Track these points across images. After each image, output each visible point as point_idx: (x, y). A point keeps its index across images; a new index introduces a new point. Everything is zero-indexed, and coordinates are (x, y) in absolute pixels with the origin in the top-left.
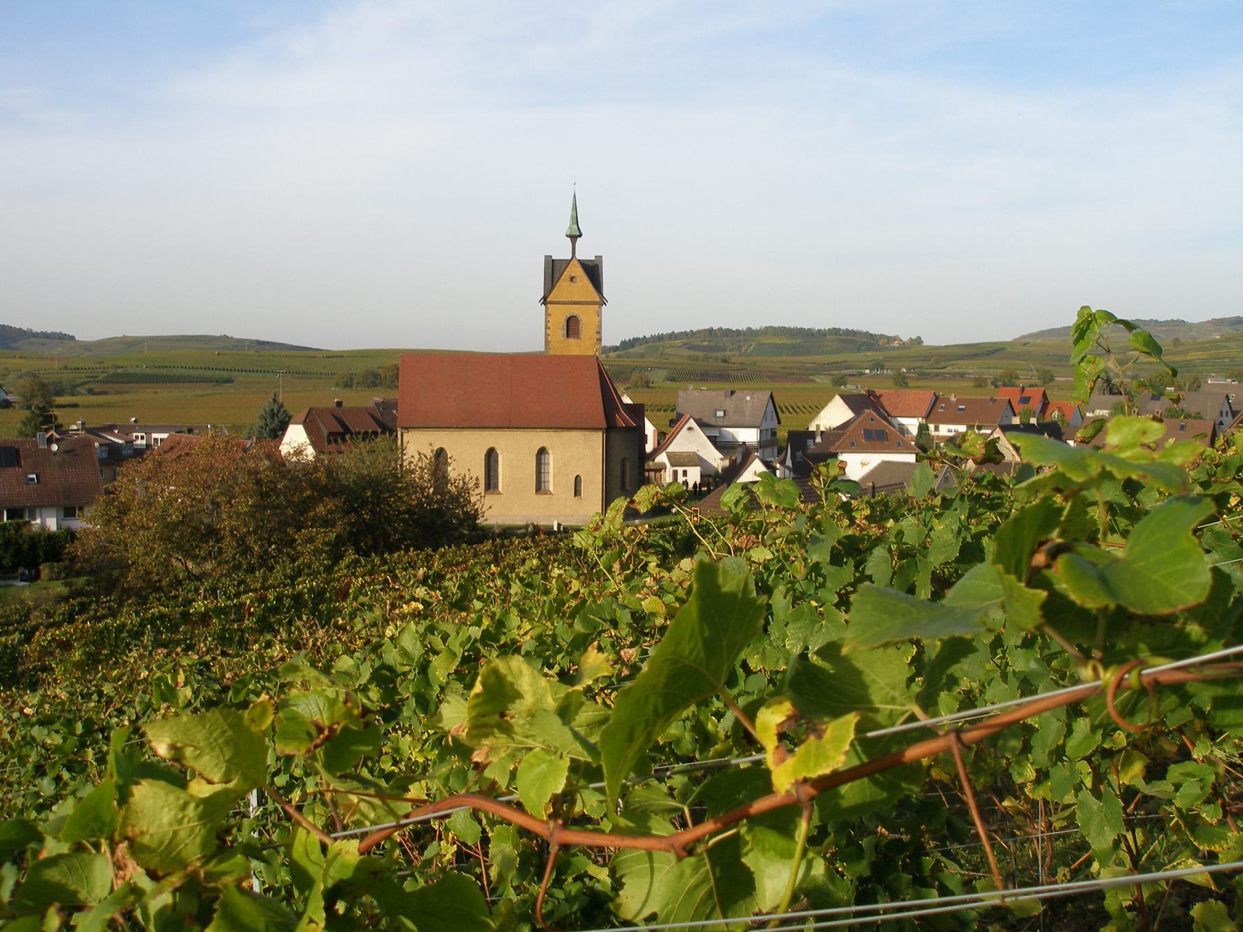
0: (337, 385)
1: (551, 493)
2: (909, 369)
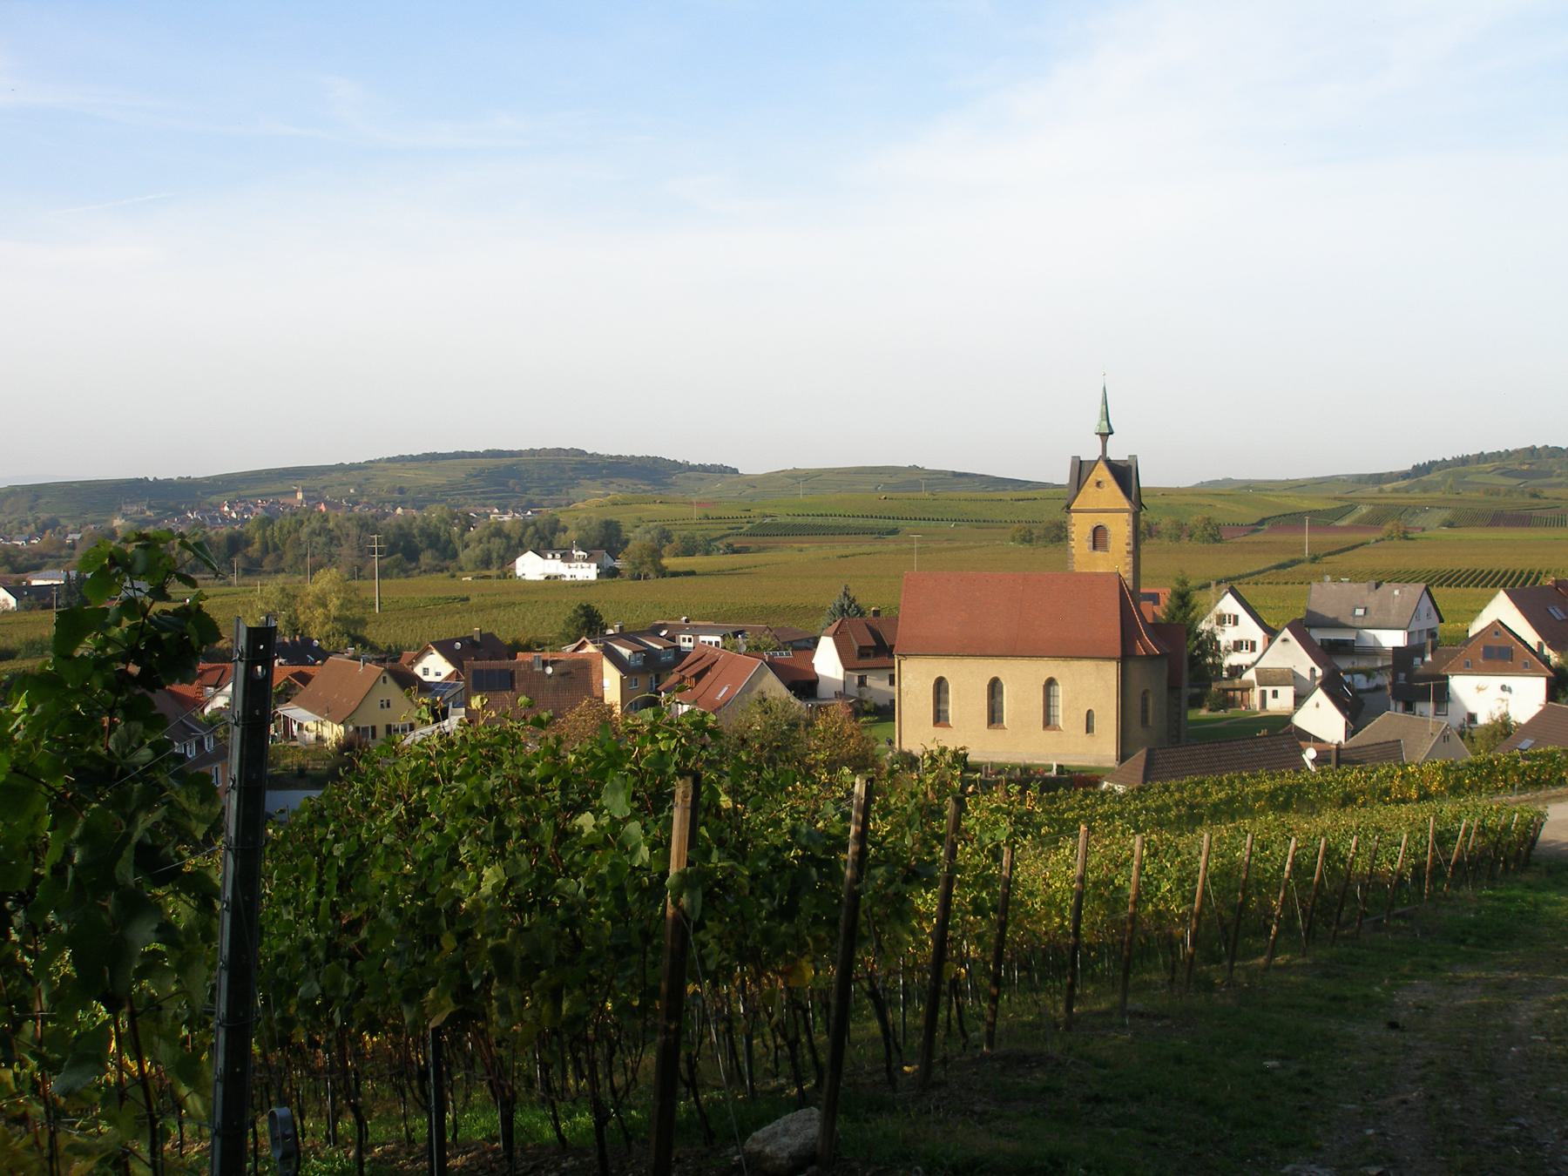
1: (1060, 729)
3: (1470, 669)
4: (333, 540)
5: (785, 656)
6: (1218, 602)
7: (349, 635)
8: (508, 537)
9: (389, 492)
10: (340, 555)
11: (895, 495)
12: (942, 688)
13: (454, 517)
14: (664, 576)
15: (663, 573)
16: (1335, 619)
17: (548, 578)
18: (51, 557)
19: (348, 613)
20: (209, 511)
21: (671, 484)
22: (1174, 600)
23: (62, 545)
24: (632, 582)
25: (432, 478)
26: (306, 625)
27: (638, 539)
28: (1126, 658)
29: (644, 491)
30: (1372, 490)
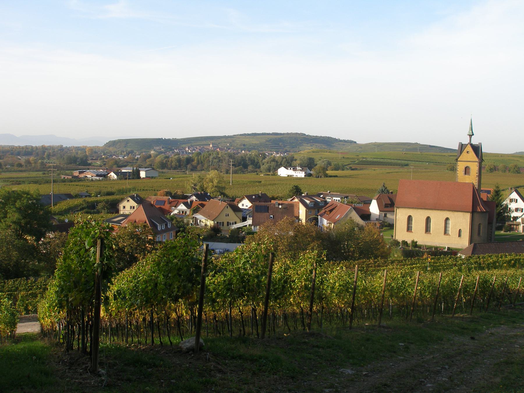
0: (447, 169)
1: (450, 235)
4: (220, 160)
5: (361, 206)
7: (220, 192)
8: (277, 162)
10: (222, 166)
12: (410, 219)
14: (327, 177)
15: (326, 176)
17: (288, 176)
18: (130, 163)
20: (181, 150)
21: (333, 146)
23: (134, 159)
24: (315, 179)
25: (254, 141)
26: (206, 188)
27: (320, 164)
28: (473, 212)
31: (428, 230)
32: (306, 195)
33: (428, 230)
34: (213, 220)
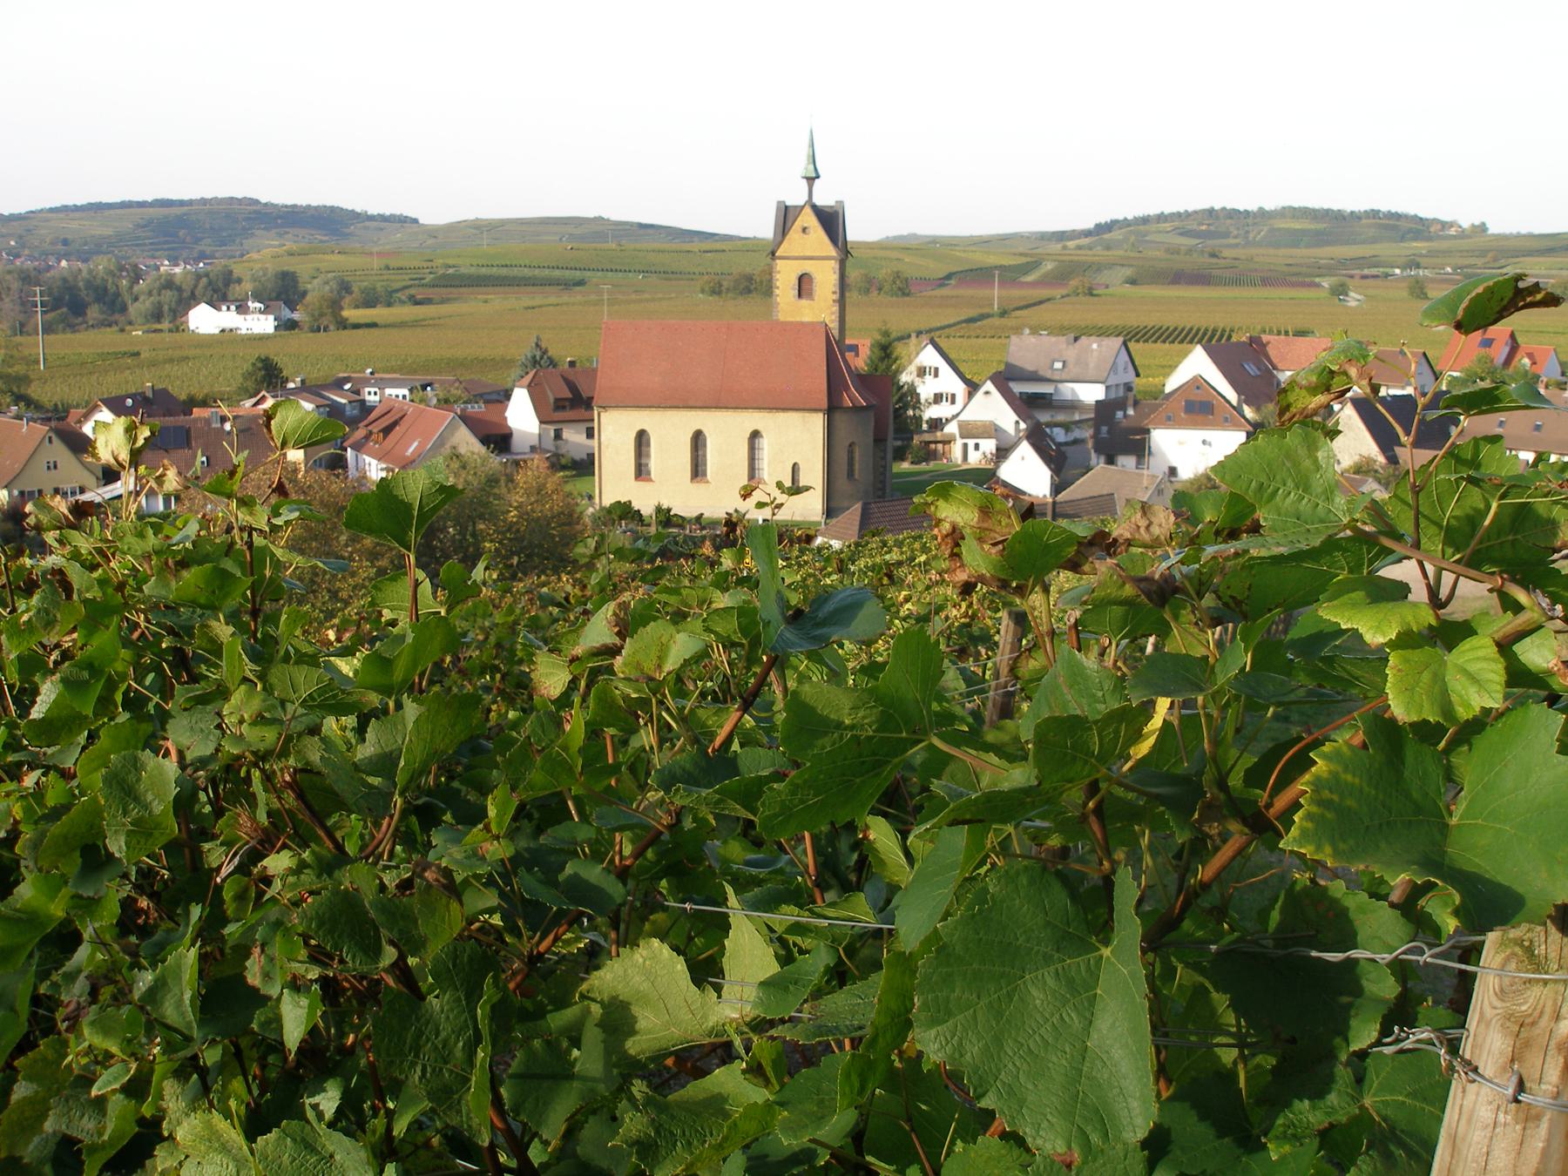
0: (703, 291)
2: (1454, 269)
3: (1170, 422)
5: (477, 409)
6: (918, 354)
7: (13, 394)
8: (180, 289)
9: (52, 243)
11: (582, 246)
12: (644, 440)
13: (122, 268)
14: (345, 328)
15: (343, 325)
16: (1035, 372)
19: (10, 370)
22: (876, 350)
24: (311, 335)
27: (316, 290)
28: (832, 409)
29: (321, 241)
30: (1056, 247)
31: (698, 470)
32: (299, 385)
33: (698, 470)
34: (6, 487)
